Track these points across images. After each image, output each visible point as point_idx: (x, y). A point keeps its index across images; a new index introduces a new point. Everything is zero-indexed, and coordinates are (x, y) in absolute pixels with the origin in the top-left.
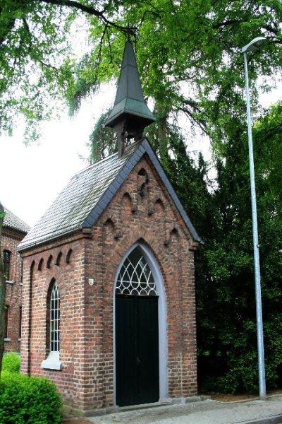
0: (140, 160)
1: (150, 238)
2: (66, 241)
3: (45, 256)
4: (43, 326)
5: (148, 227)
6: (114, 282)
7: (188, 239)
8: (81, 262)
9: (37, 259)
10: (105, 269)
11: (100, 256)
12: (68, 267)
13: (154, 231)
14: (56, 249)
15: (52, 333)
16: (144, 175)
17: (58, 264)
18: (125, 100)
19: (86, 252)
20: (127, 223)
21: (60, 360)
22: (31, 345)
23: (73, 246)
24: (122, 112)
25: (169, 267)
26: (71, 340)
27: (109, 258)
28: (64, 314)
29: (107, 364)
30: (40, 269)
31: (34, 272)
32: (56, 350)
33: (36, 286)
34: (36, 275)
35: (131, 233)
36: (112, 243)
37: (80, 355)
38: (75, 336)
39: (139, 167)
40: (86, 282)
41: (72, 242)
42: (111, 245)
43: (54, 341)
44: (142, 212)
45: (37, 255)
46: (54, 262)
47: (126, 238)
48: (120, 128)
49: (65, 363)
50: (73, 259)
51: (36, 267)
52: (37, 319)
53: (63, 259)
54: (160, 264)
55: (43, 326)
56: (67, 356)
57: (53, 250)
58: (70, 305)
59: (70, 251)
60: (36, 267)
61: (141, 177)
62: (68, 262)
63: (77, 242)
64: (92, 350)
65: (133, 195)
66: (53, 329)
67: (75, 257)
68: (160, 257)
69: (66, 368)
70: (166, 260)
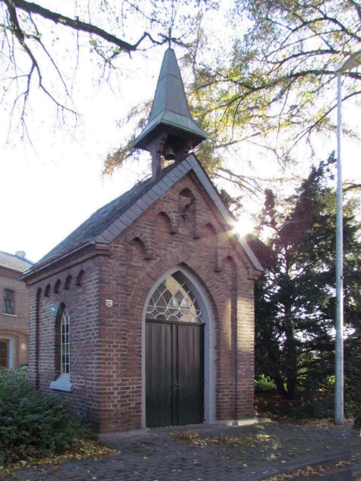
0: (183, 178)
2: (75, 262)
3: (52, 281)
4: (52, 349)
5: (192, 252)
6: (143, 306)
8: (94, 282)
9: (43, 285)
10: (131, 291)
11: (122, 277)
12: (80, 290)
13: (200, 257)
14: (64, 273)
15: (64, 356)
16: (188, 196)
17: (67, 288)
18: (163, 112)
19: (101, 270)
20: (162, 245)
21: (71, 382)
22: (39, 367)
23: (85, 266)
24: (159, 122)
25: (220, 295)
26: (84, 363)
27: (136, 280)
28: (75, 337)
29: (133, 388)
30: (47, 295)
31: (41, 299)
32: (68, 372)
33: (44, 312)
34: (43, 301)
35: (169, 257)
36: (140, 265)
37: (94, 378)
38: (88, 359)
39: (182, 186)
40: (101, 302)
41: (84, 261)
43: (66, 364)
44: (184, 235)
45: (43, 281)
46: (62, 286)
47: (161, 261)
48: (157, 145)
49: (76, 386)
50: (85, 281)
51: (43, 293)
52: (45, 343)
53: (73, 282)
55: (52, 349)
56: (80, 379)
57: (60, 274)
58: (81, 328)
59: (82, 273)
60: (43, 293)
61: (184, 198)
62: (79, 284)
63: (90, 261)
64: (111, 374)
65: (173, 216)
66: (64, 352)
67: (86, 278)
68: (208, 284)
69: (78, 390)
70: (217, 287)
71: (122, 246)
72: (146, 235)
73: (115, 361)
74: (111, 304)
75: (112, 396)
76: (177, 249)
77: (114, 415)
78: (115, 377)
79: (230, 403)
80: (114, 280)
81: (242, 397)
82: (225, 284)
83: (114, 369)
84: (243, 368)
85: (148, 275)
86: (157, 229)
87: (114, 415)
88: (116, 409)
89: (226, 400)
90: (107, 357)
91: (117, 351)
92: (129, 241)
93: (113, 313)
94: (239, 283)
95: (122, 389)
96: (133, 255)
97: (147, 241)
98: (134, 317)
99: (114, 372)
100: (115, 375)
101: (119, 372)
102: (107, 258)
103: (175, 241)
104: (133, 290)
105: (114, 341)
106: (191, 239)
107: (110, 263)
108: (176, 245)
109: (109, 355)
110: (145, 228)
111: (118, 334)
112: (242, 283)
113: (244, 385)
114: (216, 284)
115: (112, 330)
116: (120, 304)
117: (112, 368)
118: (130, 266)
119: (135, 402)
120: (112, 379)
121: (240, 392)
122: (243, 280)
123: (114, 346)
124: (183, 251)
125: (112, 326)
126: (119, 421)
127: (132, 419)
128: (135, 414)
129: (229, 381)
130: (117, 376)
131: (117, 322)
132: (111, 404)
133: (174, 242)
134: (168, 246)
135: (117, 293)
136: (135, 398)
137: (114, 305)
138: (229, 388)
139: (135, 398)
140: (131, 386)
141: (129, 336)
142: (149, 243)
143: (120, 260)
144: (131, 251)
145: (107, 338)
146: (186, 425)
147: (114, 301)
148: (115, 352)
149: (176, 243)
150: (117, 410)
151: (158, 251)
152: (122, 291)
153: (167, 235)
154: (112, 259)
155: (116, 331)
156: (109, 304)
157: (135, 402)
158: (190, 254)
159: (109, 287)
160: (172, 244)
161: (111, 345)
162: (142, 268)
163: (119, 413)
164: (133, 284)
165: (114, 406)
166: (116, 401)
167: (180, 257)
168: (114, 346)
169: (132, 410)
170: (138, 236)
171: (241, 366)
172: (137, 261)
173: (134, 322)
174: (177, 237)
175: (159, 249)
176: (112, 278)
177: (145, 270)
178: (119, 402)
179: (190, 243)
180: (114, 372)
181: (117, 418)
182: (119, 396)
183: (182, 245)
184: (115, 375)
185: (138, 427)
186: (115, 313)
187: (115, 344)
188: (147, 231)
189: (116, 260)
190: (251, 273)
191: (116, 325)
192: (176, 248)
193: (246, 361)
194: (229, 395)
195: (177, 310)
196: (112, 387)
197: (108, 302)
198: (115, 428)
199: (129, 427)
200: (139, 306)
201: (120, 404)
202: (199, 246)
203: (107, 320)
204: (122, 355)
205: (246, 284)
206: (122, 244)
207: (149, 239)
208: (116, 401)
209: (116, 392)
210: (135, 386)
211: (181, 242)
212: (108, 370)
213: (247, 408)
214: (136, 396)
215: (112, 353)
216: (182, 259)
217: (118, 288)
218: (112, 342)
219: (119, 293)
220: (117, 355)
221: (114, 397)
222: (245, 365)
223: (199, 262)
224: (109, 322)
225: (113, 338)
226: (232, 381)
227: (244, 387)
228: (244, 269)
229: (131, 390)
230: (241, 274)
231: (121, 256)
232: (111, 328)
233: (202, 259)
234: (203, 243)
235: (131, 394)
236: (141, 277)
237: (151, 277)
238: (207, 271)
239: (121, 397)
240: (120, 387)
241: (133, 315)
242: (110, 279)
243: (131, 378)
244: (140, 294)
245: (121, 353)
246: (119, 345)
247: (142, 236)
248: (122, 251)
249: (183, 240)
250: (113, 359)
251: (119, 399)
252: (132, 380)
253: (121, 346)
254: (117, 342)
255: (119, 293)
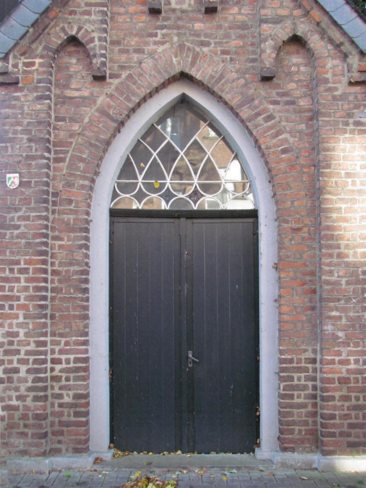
1: (210, 71)
5: (203, 44)
7: (345, 56)
13: (224, 52)
20: (134, 41)
27: (76, 127)
29: (68, 361)
35: (148, 64)
36: (86, 93)
42: (84, 98)
44: (183, 11)
47: (130, 77)
54: (220, 99)
64: (15, 329)
68: (245, 113)
70: (270, 118)
71: (41, 60)
72: (88, 27)
73: (22, 301)
74: (17, 181)
75: (15, 376)
76: (167, 46)
77: (20, 419)
78: (22, 337)
79: (310, 408)
80: (24, 132)
81: (337, 394)
82: (291, 107)
83: (21, 320)
84: (340, 318)
85: (103, 112)
86: (122, 10)
87: (20, 419)
88: (24, 406)
89: (296, 400)
90: (7, 293)
91: (28, 280)
92: (55, 47)
93: (20, 200)
94: (324, 97)
95: (35, 361)
96: (71, 76)
97: (92, 40)
98: (72, 207)
99: (19, 325)
100: (22, 332)
101: (31, 326)
102: (12, 88)
103: (162, 28)
104: (71, 149)
105: (22, 259)
106: (201, 16)
107: (17, 99)
108: (164, 36)
109: (11, 289)
110: (89, 13)
111: (28, 244)
112: (334, 98)
113: (341, 362)
114: (265, 110)
115: (18, 237)
116: (33, 181)
117: (17, 317)
118: (64, 100)
119: (71, 393)
120: (16, 339)
121: (330, 381)
122: (336, 89)
123: (21, 271)
124: (181, 47)
125: (18, 227)
126: (30, 431)
127: (65, 429)
128: (73, 419)
129: (305, 351)
130: (26, 335)
131: (27, 218)
132: (14, 394)
133: (159, 31)
134: (147, 44)
135: (28, 157)
136: (71, 383)
137: (21, 184)
138: (306, 370)
139: (71, 383)
140: (63, 357)
141: (61, 247)
142: (97, 42)
143: (36, 89)
144: (67, 68)
145: (8, 253)
146: (203, 455)
147: (21, 176)
148: (23, 284)
149: (164, 31)
150: (26, 408)
151: (124, 57)
152: (39, 153)
153: (145, 18)
154: (21, 90)
155: (25, 237)
156: (13, 182)
157: (71, 393)
158: (198, 49)
159: (12, 148)
160: (156, 35)
161: (16, 267)
162: (90, 100)
163: (30, 414)
164: (72, 136)
165: (19, 398)
166: (23, 388)
167: (174, 60)
168: (21, 271)
169: (66, 410)
170: (74, 33)
171: (334, 313)
172: (80, 86)
173: (72, 217)
174: (168, 19)
175: (127, 51)
176: (19, 128)
177: (95, 102)
178: (29, 389)
179: (198, 26)
180: (19, 325)
181: (26, 426)
182: (31, 377)
183: (178, 35)
184: (22, 332)
185: (81, 447)
186: (26, 201)
187: (23, 266)
188: (93, 17)
189: (29, 90)
190: (355, 66)
191: (25, 226)
192: (163, 43)
193: (348, 300)
194: (305, 387)
195: (192, 184)
196: (15, 358)
197: (10, 178)
198: (22, 447)
199: (58, 446)
200: (81, 182)
201: (32, 394)
202: (220, 27)
203: (9, 216)
204: (37, 289)
205: (344, 97)
206: (42, 57)
207: (96, 35)
208: (23, 388)
209: (23, 368)
210: (72, 357)
211: (178, 28)
212: (9, 321)
213: (352, 426)
214: (76, 379)
215: (16, 285)
216: (178, 64)
217: (30, 148)
218: (18, 263)
219: (33, 158)
220: (26, 289)
221: (20, 380)
222: (344, 310)
223: (222, 65)
224: (12, 219)
225: (18, 253)
226: (315, 351)
227: (344, 368)
228: (337, 62)
229: (64, 366)
230: (329, 76)
231: (39, 81)
232: (16, 232)
233: (228, 57)
234: (231, 18)
235: (64, 375)
236: (86, 120)
237: (108, 115)
238: (242, 81)
239: (35, 380)
240: (31, 358)
241: (70, 202)
242: (15, 132)
243: (63, 340)
244: (84, 156)
245: (35, 284)
246: (31, 267)
247: (83, 31)
248: (41, 69)
249: (180, 23)
250: (18, 299)
251: (30, 384)
252: (67, 343)
253: (36, 271)
254: (26, 262)
255: (33, 158)
